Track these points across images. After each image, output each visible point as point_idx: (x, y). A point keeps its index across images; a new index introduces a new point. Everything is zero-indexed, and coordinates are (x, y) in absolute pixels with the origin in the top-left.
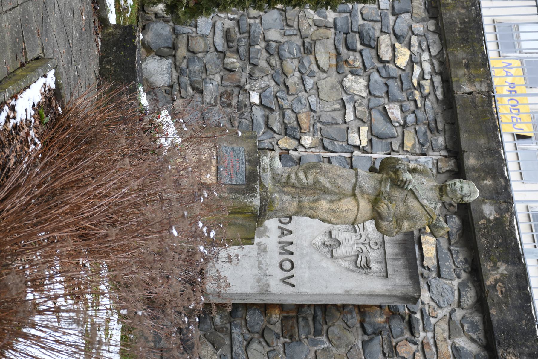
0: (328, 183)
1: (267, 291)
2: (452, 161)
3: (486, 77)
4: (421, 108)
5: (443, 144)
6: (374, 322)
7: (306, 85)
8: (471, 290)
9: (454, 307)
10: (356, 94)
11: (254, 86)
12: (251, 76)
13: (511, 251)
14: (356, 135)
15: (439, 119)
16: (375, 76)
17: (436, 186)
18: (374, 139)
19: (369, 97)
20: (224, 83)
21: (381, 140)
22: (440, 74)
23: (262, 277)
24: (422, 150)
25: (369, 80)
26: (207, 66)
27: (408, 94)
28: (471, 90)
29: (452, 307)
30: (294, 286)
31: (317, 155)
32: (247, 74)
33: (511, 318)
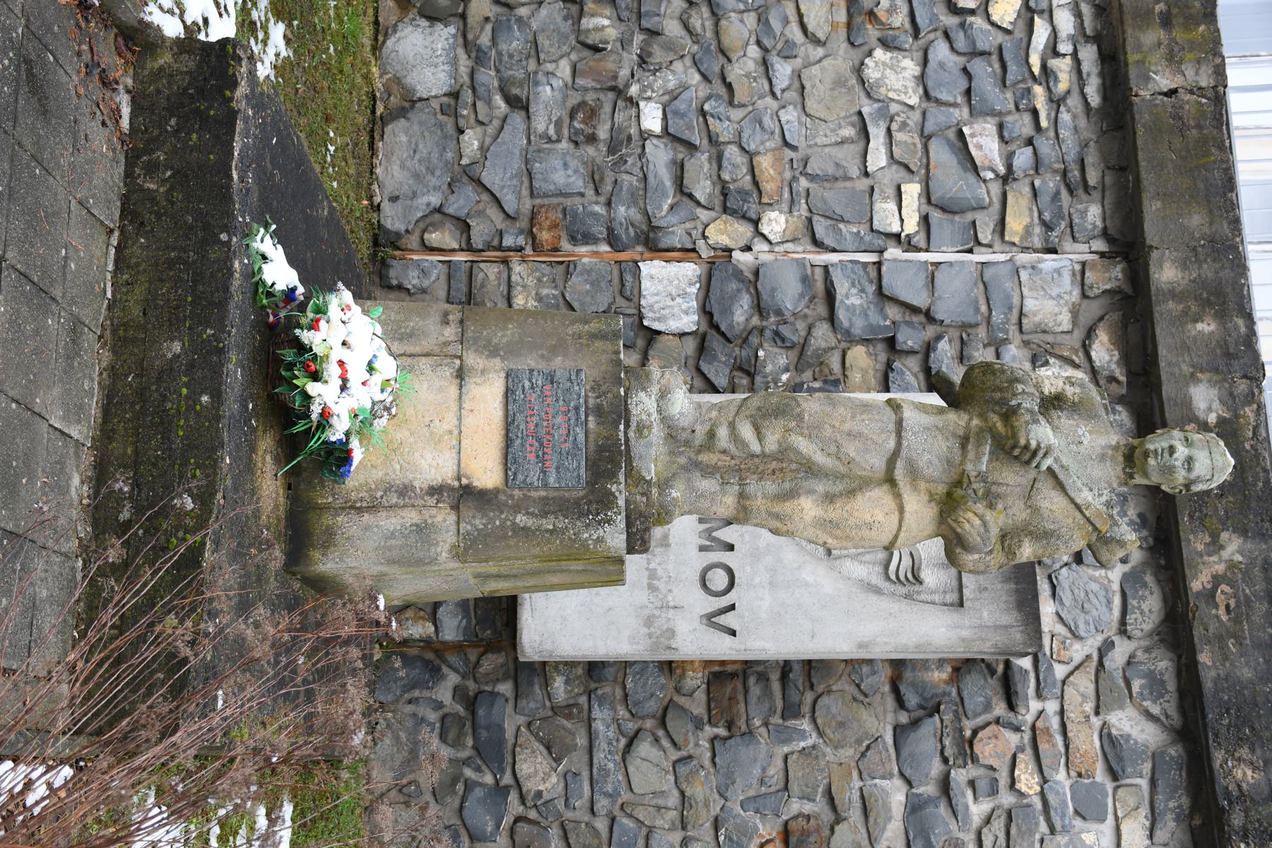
0: (819, 452)
1: (670, 648)
2: (1119, 268)
3: (1213, 49)
4: (1047, 129)
5: (1099, 224)
6: (924, 682)
7: (774, 80)
8: (1152, 593)
9: (1110, 634)
10: (893, 100)
11: (650, 86)
12: (642, 61)
13: (1253, 504)
14: (892, 206)
15: (1092, 158)
16: (941, 51)
17: (1116, 448)
18: (935, 215)
19: (924, 105)
20: (580, 82)
21: (951, 216)
22: (1097, 39)
23: (657, 613)
24: (1047, 241)
25: (925, 62)
26: (540, 39)
27: (1018, 94)
28: (1174, 86)
29: (1105, 636)
30: (733, 633)
31: (797, 260)
32: (635, 57)
33: (1247, 673)
